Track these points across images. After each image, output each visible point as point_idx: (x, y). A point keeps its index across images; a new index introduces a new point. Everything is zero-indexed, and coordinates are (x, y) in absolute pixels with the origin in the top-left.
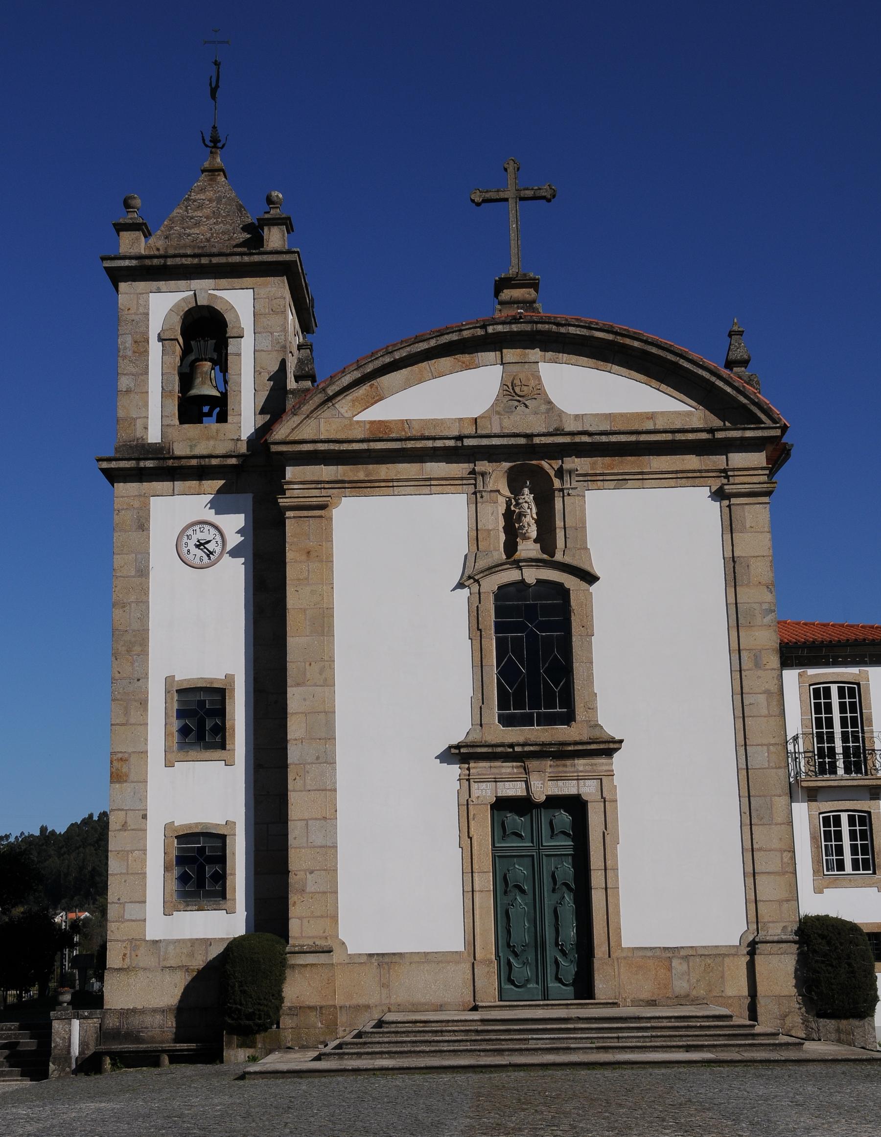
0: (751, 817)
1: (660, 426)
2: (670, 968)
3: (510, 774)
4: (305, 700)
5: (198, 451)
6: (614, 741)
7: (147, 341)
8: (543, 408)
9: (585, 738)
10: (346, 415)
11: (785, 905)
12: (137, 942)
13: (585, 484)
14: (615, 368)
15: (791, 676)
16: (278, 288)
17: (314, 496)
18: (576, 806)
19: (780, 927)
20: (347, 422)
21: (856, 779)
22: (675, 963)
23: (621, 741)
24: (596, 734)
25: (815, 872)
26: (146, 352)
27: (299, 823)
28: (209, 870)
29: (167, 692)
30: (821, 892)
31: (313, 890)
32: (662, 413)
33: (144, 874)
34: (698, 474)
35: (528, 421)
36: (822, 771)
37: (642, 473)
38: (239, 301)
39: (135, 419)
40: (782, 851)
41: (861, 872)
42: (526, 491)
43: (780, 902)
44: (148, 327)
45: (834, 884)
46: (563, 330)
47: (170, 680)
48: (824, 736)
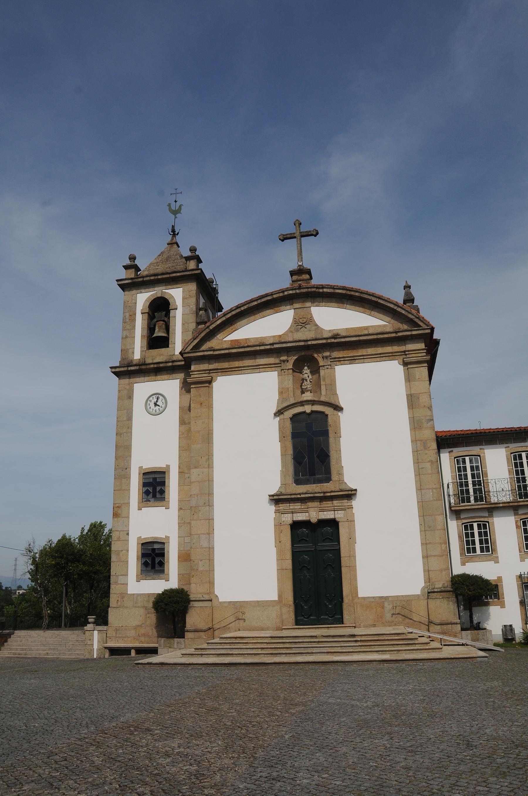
0: (426, 527)
1: (371, 331)
2: (383, 607)
3: (299, 509)
4: (199, 475)
5: (155, 361)
6: (352, 490)
7: (135, 314)
8: (314, 328)
9: (337, 489)
10: (220, 338)
11: (444, 572)
12: (124, 595)
13: (335, 363)
14: (348, 306)
15: (446, 457)
16: (192, 287)
17: (205, 377)
18: (334, 523)
19: (442, 581)
20: (220, 341)
21: (482, 504)
22: (386, 604)
23: (356, 490)
24: (343, 487)
25: (461, 554)
27: (195, 536)
28: (157, 560)
29: (139, 474)
31: (202, 569)
33: (128, 561)
34: (391, 354)
36: (463, 502)
37: (363, 356)
38: (177, 294)
39: (128, 349)
40: (441, 544)
41: (485, 553)
42: (306, 368)
43: (441, 571)
44: (136, 309)
45: (471, 560)
46: (321, 290)
48: (462, 484)
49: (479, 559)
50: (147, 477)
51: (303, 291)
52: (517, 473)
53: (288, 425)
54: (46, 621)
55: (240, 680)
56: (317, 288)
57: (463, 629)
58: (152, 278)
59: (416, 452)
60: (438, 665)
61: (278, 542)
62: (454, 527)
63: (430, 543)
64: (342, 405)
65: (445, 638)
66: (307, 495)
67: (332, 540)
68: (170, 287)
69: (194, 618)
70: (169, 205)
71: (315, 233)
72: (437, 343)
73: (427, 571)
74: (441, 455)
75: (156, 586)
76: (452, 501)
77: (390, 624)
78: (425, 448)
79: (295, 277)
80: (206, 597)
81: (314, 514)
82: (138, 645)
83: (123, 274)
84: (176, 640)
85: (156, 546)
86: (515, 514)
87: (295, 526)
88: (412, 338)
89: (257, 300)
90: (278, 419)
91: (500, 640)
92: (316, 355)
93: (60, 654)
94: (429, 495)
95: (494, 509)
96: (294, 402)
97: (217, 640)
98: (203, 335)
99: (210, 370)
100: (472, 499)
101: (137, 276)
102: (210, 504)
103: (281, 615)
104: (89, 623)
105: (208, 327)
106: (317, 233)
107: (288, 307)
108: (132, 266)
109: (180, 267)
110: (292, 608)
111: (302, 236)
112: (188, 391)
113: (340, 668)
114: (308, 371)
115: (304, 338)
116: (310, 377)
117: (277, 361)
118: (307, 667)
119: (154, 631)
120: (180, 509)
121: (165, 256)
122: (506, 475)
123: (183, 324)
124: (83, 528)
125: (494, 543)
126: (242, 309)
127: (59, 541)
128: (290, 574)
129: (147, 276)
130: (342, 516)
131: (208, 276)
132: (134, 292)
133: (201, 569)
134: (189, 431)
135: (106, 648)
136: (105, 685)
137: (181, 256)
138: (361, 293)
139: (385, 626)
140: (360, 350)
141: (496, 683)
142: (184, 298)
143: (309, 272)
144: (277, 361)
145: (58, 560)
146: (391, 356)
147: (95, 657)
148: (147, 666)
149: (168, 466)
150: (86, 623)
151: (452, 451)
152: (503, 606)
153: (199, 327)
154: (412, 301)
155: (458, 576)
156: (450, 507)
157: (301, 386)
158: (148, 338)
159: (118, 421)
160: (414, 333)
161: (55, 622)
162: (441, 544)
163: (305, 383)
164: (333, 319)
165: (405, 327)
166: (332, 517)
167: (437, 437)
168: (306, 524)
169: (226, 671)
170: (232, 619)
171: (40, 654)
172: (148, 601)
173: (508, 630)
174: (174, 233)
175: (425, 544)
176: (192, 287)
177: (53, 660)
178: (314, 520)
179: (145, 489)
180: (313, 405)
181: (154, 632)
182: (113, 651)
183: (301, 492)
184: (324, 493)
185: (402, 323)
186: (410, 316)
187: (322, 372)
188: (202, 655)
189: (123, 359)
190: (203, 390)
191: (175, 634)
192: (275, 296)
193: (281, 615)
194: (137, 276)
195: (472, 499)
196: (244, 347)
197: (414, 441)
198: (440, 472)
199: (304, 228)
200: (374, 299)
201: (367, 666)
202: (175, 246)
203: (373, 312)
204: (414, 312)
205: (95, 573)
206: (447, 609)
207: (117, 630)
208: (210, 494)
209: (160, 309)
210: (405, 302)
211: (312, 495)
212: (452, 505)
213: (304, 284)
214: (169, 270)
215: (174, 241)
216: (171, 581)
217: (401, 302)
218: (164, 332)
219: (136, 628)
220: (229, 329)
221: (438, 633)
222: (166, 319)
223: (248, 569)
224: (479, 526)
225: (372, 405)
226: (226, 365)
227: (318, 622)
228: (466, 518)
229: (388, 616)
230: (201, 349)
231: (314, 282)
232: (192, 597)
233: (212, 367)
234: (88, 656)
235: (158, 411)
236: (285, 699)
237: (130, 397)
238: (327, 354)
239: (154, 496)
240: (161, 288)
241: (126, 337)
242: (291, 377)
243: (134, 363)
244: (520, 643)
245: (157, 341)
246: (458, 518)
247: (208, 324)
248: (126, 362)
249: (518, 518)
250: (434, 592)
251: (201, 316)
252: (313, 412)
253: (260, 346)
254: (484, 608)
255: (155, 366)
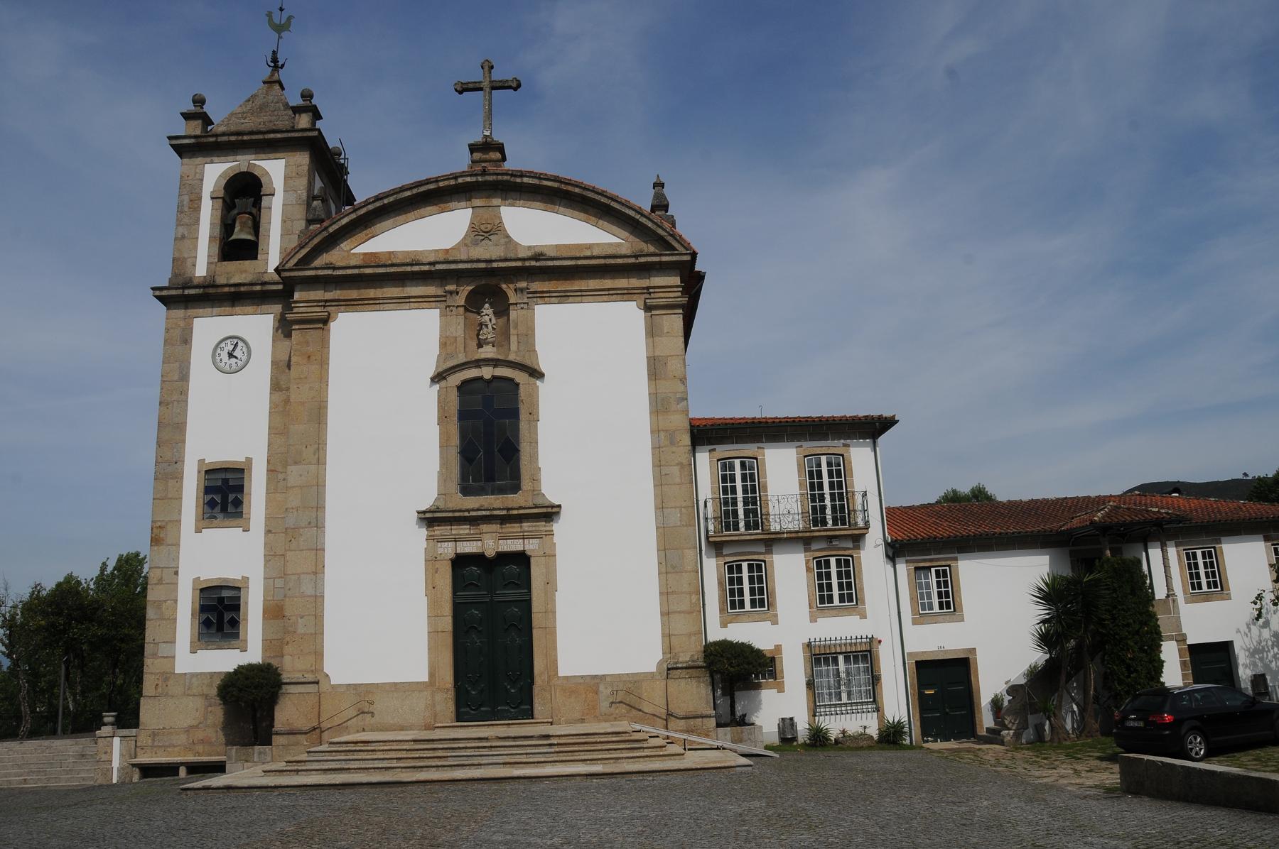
0: (669, 565)
1: (595, 253)
5: (232, 281)
6: (553, 507)
7: (200, 199)
8: (503, 241)
9: (530, 504)
12: (168, 676)
15: (704, 460)
18: (522, 559)
19: (690, 652)
21: (756, 534)
22: (602, 688)
23: (559, 506)
24: (539, 501)
26: (199, 208)
27: (293, 577)
28: (227, 617)
30: (725, 626)
32: (598, 244)
33: (175, 619)
35: (488, 251)
38: (275, 170)
40: (690, 594)
42: (487, 305)
43: (690, 635)
45: (736, 619)
46: (518, 180)
47: (201, 462)
49: (749, 618)
50: (213, 476)
51: (489, 180)
52: (812, 488)
53: (454, 397)
54: (26, 726)
55: (355, 810)
56: (512, 175)
57: (719, 725)
58: (233, 138)
59: (657, 449)
60: (676, 779)
61: (431, 587)
62: (712, 568)
63: (674, 592)
64: (543, 368)
65: (691, 738)
66: (479, 513)
67: (518, 586)
68: (263, 156)
69: (287, 713)
70: (270, 15)
71: (514, 85)
72: (700, 277)
73: (667, 636)
74: (697, 455)
75: (225, 660)
76: (711, 527)
77: (607, 718)
78: (672, 443)
79: (477, 156)
80: (310, 677)
81: (490, 543)
82: (191, 758)
83: (182, 128)
84: (257, 748)
85: (225, 594)
86: (806, 550)
87: (460, 562)
88: (663, 270)
89: (411, 189)
90: (437, 387)
91: (775, 740)
92: (504, 286)
93: (49, 779)
94: (675, 517)
95: (774, 541)
96: (464, 360)
97: (325, 747)
98: (316, 241)
99: (326, 301)
100: (742, 524)
101: (206, 134)
102: (318, 525)
103: (434, 705)
104: (105, 725)
105: (326, 228)
106: (519, 86)
107: (463, 204)
108: (197, 114)
109: (283, 123)
110: (451, 695)
111: (494, 88)
112: (288, 335)
113: (522, 787)
114: (490, 311)
115: (487, 257)
116: (494, 321)
117: (440, 292)
118: (469, 787)
119: (221, 734)
120: (268, 532)
121: (258, 102)
122: (796, 490)
123: (284, 221)
124: (104, 564)
125: (771, 594)
126: (386, 201)
127: (59, 585)
128: (448, 640)
129: (223, 134)
130: (536, 547)
131: (332, 143)
132: (199, 160)
133: (301, 630)
134: (287, 401)
135: (134, 765)
136: (119, 827)
137: (286, 106)
138: (584, 189)
139: (599, 721)
140: (577, 282)
141: (757, 803)
142: (287, 178)
143: (500, 148)
144: (440, 292)
145: (52, 619)
146: (626, 294)
147: (115, 781)
148: (202, 793)
149: (249, 460)
150: (100, 724)
151: (714, 450)
152: (781, 689)
153: (311, 227)
154: (665, 207)
155: (715, 643)
156: (707, 537)
157: (478, 335)
158: (221, 241)
159: (163, 381)
160: (665, 259)
161: (45, 727)
162: (690, 594)
163: (485, 330)
164: (534, 228)
165: (652, 249)
166: (520, 548)
167: (692, 426)
168: (478, 558)
169: (336, 797)
170: (352, 712)
171: (9, 782)
172: (210, 685)
173: (787, 725)
174: (276, 64)
175: (665, 594)
176: (303, 159)
177: (34, 792)
178: (490, 553)
179: (209, 497)
180: (495, 366)
181: (217, 736)
182: (148, 771)
183: (470, 506)
184: (508, 509)
185: (646, 242)
186: (660, 231)
187: (513, 314)
188: (298, 771)
189: (175, 275)
190: (313, 335)
191: (256, 738)
192: (441, 184)
193: (434, 705)
194: (206, 134)
195: (742, 524)
196: (385, 266)
197: (655, 431)
198: (693, 482)
199: (497, 75)
200: (604, 200)
201: (566, 783)
202: (277, 87)
203: (601, 222)
204: (667, 225)
205: (122, 640)
206: (695, 695)
207: (154, 735)
208: (320, 507)
209: (244, 194)
210: (654, 208)
211: (488, 513)
212: (711, 533)
213: (491, 168)
214: (262, 128)
215: (276, 77)
216: (253, 653)
217: (647, 208)
218: (249, 233)
219: (188, 730)
220: (362, 235)
221: (682, 731)
222: (254, 211)
223: (379, 629)
224: (750, 568)
225: (592, 371)
226: (354, 294)
227: (493, 715)
228: (730, 556)
229: (604, 706)
230: (313, 265)
231: (508, 165)
232: (285, 677)
233: (329, 295)
234: (101, 781)
235: (234, 366)
236: (423, 837)
237: (186, 340)
238: (523, 284)
239: (224, 510)
240: (247, 157)
241: (183, 237)
242: (461, 320)
243: (195, 282)
244: (805, 744)
245: (236, 248)
246: (719, 555)
247: (325, 224)
248: (180, 281)
249: (810, 555)
250: (677, 668)
251: (315, 209)
252: (494, 378)
253: (412, 265)
254: (753, 692)
255: (232, 289)
